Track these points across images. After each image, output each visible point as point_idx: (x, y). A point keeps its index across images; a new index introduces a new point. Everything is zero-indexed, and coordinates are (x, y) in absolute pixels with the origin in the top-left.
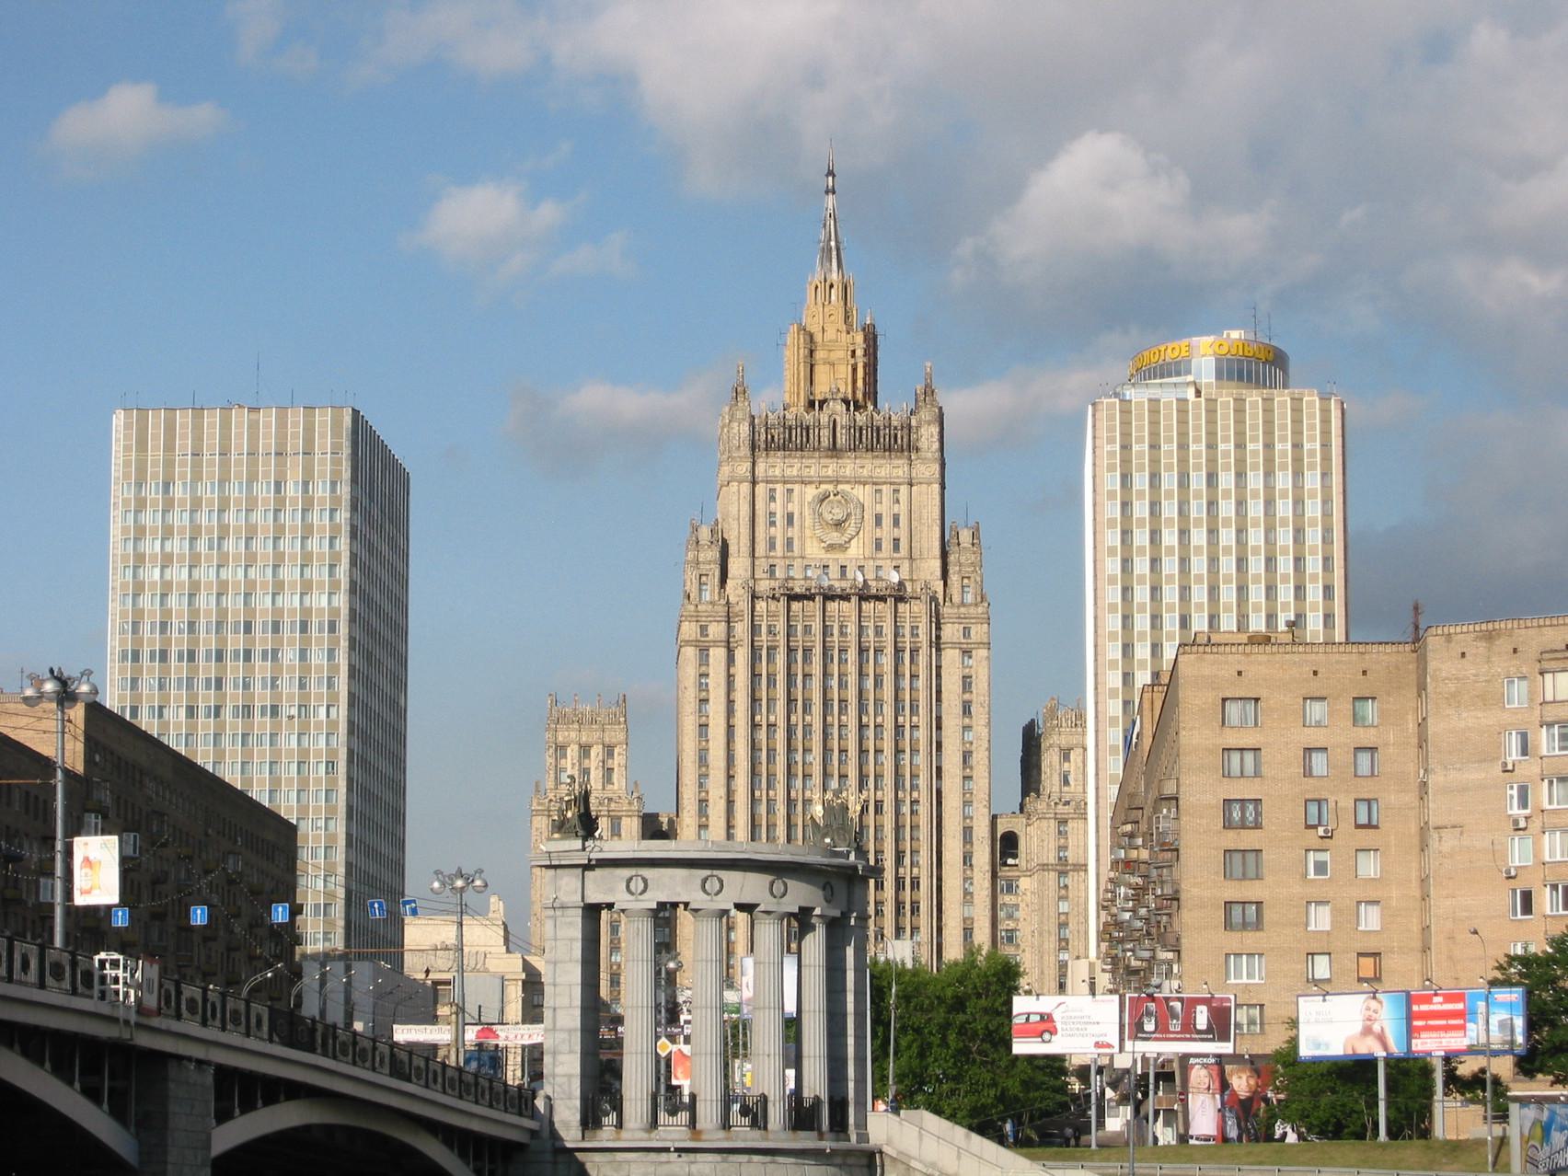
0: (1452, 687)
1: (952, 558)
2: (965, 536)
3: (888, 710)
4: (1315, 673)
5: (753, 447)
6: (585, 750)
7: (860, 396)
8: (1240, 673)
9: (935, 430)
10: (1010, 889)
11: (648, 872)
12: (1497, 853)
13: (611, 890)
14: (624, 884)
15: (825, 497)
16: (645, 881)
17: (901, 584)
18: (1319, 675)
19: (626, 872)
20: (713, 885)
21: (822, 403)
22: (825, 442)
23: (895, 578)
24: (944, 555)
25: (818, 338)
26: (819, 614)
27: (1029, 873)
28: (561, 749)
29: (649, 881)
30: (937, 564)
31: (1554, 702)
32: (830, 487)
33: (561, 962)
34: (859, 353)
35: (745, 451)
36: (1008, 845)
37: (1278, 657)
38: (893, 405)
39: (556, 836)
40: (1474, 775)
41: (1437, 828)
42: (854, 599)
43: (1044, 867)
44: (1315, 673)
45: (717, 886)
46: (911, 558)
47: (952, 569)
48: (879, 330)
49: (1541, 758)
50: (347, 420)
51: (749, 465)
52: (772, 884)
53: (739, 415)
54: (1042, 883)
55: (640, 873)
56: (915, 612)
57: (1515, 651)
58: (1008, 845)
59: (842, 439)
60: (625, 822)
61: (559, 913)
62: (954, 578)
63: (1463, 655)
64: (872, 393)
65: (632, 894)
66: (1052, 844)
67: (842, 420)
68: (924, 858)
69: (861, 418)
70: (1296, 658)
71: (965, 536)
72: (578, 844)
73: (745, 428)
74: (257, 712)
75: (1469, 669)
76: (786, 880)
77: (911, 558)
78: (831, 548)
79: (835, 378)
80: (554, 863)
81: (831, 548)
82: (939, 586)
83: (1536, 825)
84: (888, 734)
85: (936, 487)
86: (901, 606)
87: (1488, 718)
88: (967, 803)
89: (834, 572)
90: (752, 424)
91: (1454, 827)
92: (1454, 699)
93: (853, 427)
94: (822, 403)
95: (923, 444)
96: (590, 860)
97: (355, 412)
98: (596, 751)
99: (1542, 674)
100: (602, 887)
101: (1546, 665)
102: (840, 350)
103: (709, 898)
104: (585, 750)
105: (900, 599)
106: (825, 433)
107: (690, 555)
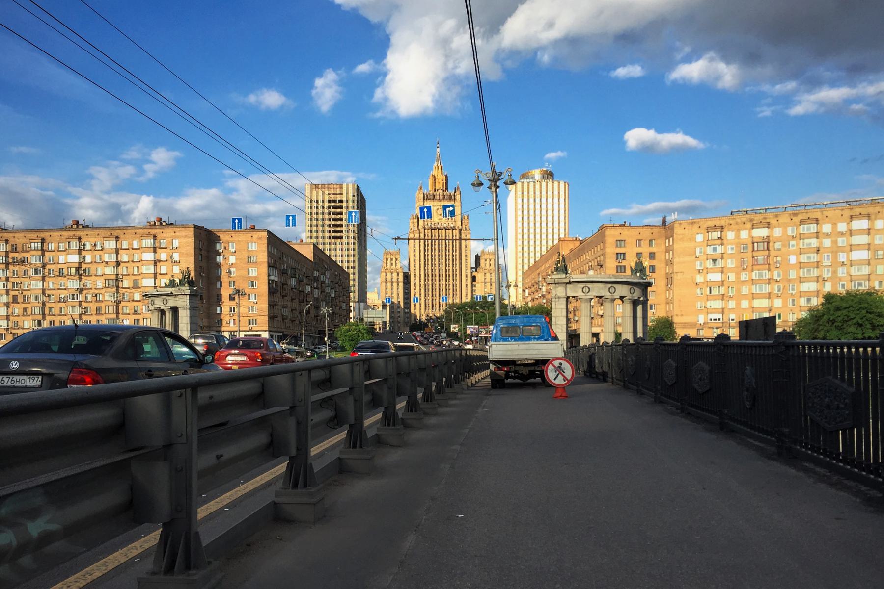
0: (681, 236)
1: (463, 221)
2: (466, 217)
3: (451, 251)
4: (640, 234)
5: (424, 199)
6: (392, 260)
7: (444, 189)
8: (621, 234)
9: (460, 196)
10: (475, 286)
11: (590, 286)
12: (693, 279)
13: (576, 292)
14: (581, 290)
15: (438, 209)
16: (589, 288)
17: (454, 226)
18: (843, 217)
19: (582, 285)
20: (612, 290)
21: (437, 190)
22: (438, 198)
23: (452, 225)
24: (461, 221)
25: (436, 177)
26: (437, 233)
27: (478, 283)
28: (387, 259)
29: (590, 289)
30: (460, 223)
31: (711, 240)
32: (439, 207)
33: (558, 317)
34: (444, 180)
35: (422, 200)
36: (474, 279)
37: (630, 230)
38: (451, 191)
39: (555, 273)
40: (687, 259)
41: (676, 273)
42: (444, 230)
43: (482, 282)
44: (640, 234)
45: (587, 290)
46: (455, 221)
47: (463, 224)
48: (448, 176)
49: (707, 254)
50: (356, 187)
51: (423, 203)
52: (630, 289)
53: (421, 193)
54: (481, 285)
55: (587, 286)
56: (456, 232)
57: (700, 227)
58: (474, 279)
59: (441, 198)
60: (388, 274)
61: (557, 300)
62: (463, 225)
63: (685, 228)
64: (447, 189)
65: (584, 293)
66: (483, 278)
67: (441, 194)
68: (458, 280)
69: (445, 193)
70: (635, 230)
71: (466, 217)
72: (564, 276)
73: (422, 195)
74: (332, 250)
75: (686, 231)
76: (634, 287)
77: (455, 221)
78: (439, 219)
79: (439, 186)
80: (556, 282)
81: (439, 219)
82: (461, 227)
83: (705, 271)
84: (430, 256)
85: (460, 207)
86: (454, 231)
87: (692, 244)
88: (466, 270)
89: (440, 224)
90: (424, 195)
91: (681, 272)
92: (682, 240)
93: (443, 195)
94: (437, 190)
95: (457, 198)
96: (570, 281)
97: (357, 185)
98: (394, 259)
99: (708, 232)
100: (575, 291)
101: (709, 230)
102: (441, 179)
103: (584, 294)
104: (392, 260)
105: (453, 229)
106: (438, 196)
107: (412, 221)
